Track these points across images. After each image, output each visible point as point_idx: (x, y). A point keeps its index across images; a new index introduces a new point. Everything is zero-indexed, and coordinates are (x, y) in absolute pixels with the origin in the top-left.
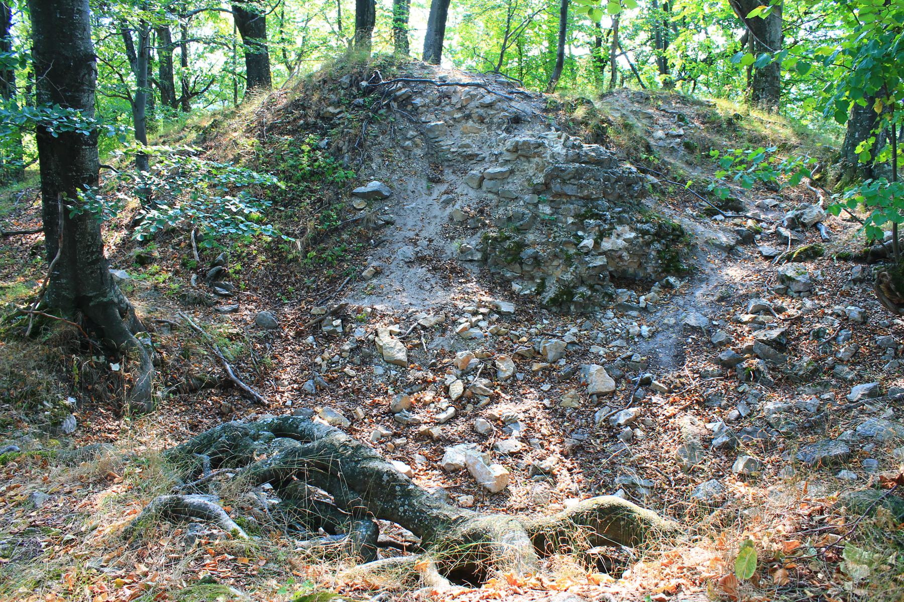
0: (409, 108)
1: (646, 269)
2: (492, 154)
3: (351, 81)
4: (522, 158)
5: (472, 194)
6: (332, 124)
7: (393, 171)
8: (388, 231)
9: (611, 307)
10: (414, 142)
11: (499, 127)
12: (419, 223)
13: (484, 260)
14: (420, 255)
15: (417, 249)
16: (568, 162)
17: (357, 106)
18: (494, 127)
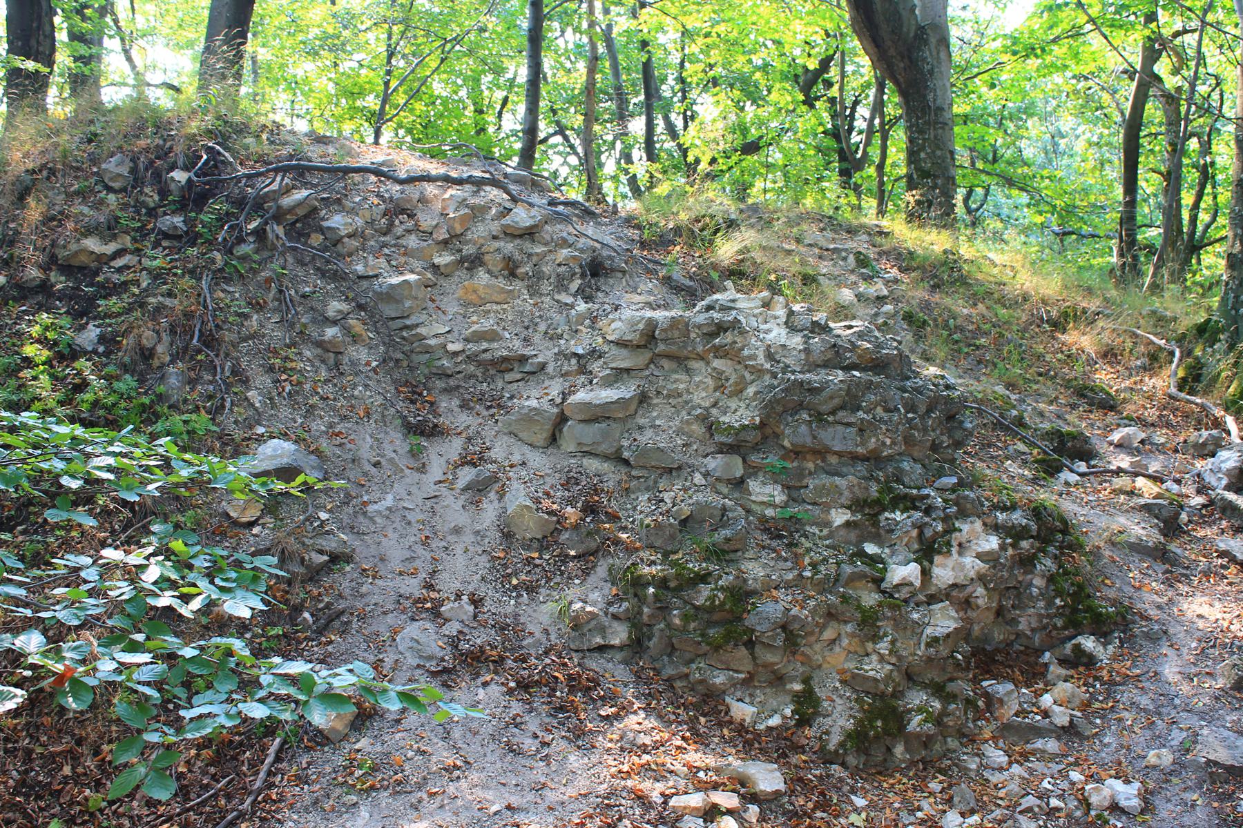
0: (316, 239)
1: (1014, 622)
2: (563, 356)
3: (134, 171)
4: (666, 363)
5: (537, 460)
6: (101, 286)
7: (310, 411)
8: (344, 579)
9: (987, 734)
10: (347, 330)
11: (561, 285)
12: (420, 550)
13: (636, 646)
14: (464, 647)
15: (452, 628)
16: (812, 367)
17: (166, 236)
18: (546, 287)
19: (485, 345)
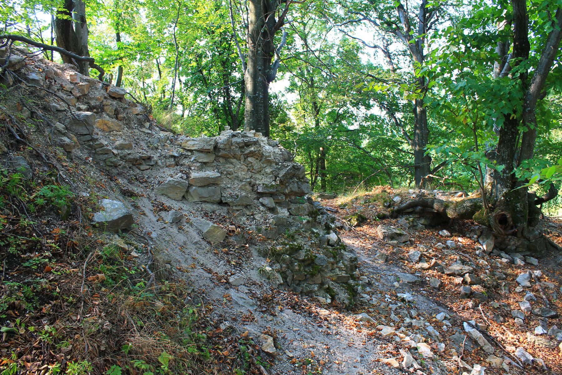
4: (221, 160)
19: (127, 151)
